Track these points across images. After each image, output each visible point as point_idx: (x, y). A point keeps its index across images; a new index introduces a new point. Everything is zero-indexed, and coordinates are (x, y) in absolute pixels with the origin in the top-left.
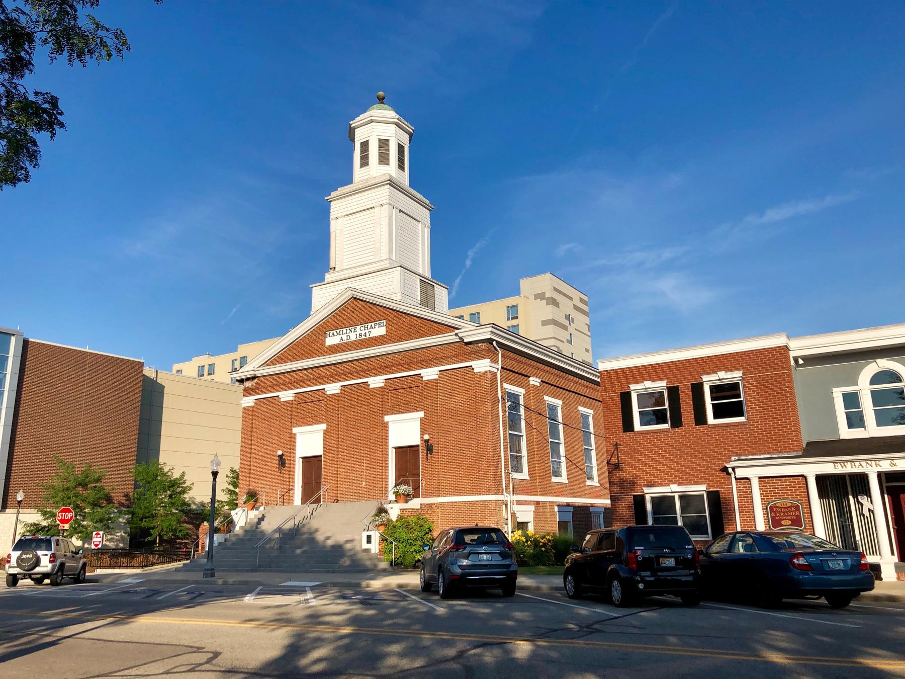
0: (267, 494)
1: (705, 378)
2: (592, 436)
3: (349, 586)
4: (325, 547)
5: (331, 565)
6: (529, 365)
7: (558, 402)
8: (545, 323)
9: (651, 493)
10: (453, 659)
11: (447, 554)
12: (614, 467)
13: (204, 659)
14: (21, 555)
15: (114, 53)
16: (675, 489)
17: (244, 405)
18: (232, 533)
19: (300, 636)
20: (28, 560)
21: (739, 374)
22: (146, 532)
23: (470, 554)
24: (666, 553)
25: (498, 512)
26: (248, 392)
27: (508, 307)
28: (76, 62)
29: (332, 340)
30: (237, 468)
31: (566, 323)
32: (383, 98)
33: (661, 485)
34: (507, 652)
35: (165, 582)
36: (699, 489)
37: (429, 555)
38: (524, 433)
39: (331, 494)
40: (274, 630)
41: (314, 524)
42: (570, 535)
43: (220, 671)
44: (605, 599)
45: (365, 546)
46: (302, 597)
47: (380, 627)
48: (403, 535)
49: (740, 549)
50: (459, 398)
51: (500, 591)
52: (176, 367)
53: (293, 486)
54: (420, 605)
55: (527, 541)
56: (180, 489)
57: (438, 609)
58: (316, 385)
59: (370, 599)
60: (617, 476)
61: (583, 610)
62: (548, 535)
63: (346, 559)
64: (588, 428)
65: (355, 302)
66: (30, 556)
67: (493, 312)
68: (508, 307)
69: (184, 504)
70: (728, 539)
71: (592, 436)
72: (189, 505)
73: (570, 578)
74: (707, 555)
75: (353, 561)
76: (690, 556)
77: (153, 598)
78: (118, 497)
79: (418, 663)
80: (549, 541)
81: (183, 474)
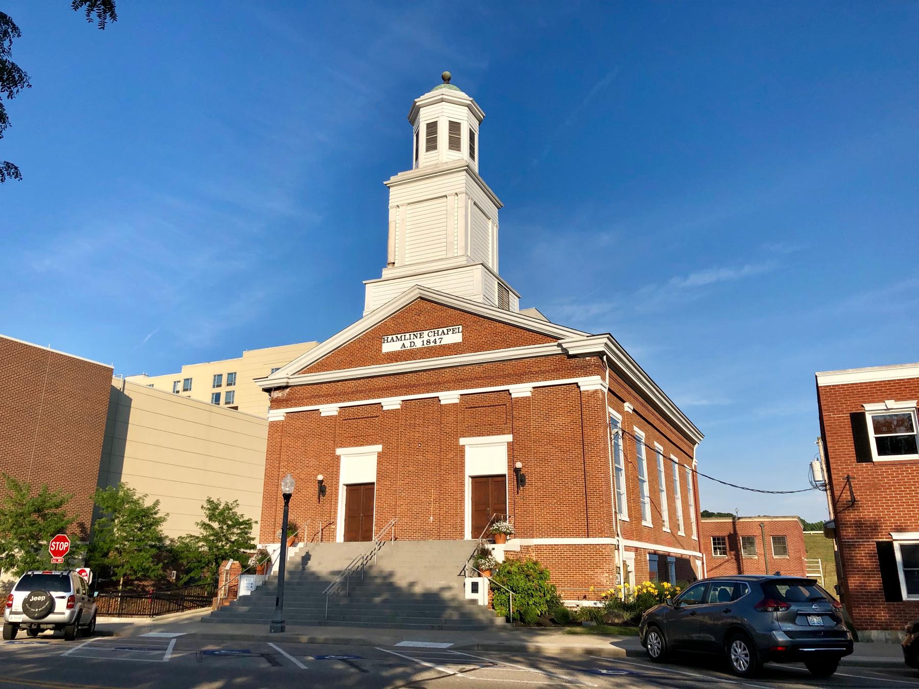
4: (413, 595)
9: (900, 539)
14: (30, 596)
17: (271, 419)
20: (39, 604)
21: (913, 404)
25: (610, 558)
26: (276, 404)
29: (389, 347)
32: (449, 79)
41: (386, 565)
45: (469, 595)
48: (522, 583)
50: (559, 421)
66: (43, 598)
75: (463, 615)
81: (157, 503)
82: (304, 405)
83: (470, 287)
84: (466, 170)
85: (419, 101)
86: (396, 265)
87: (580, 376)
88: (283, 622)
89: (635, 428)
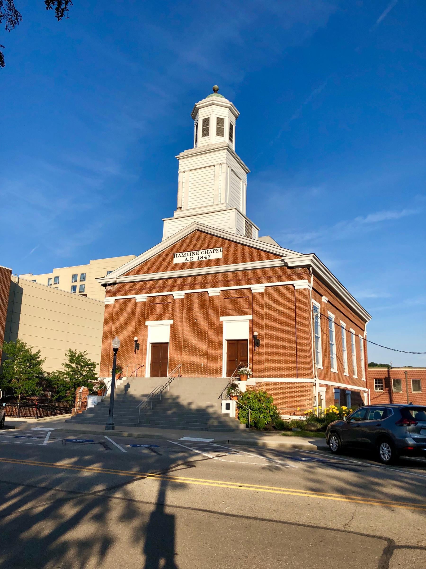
4: (191, 410)
17: (106, 303)
26: (109, 294)
27: (73, 275)
29: (178, 260)
32: (217, 90)
45: (224, 411)
48: (256, 405)
50: (281, 307)
68: (73, 275)
81: (39, 351)
84: (227, 149)
86: (182, 209)
88: (113, 424)
89: (329, 312)
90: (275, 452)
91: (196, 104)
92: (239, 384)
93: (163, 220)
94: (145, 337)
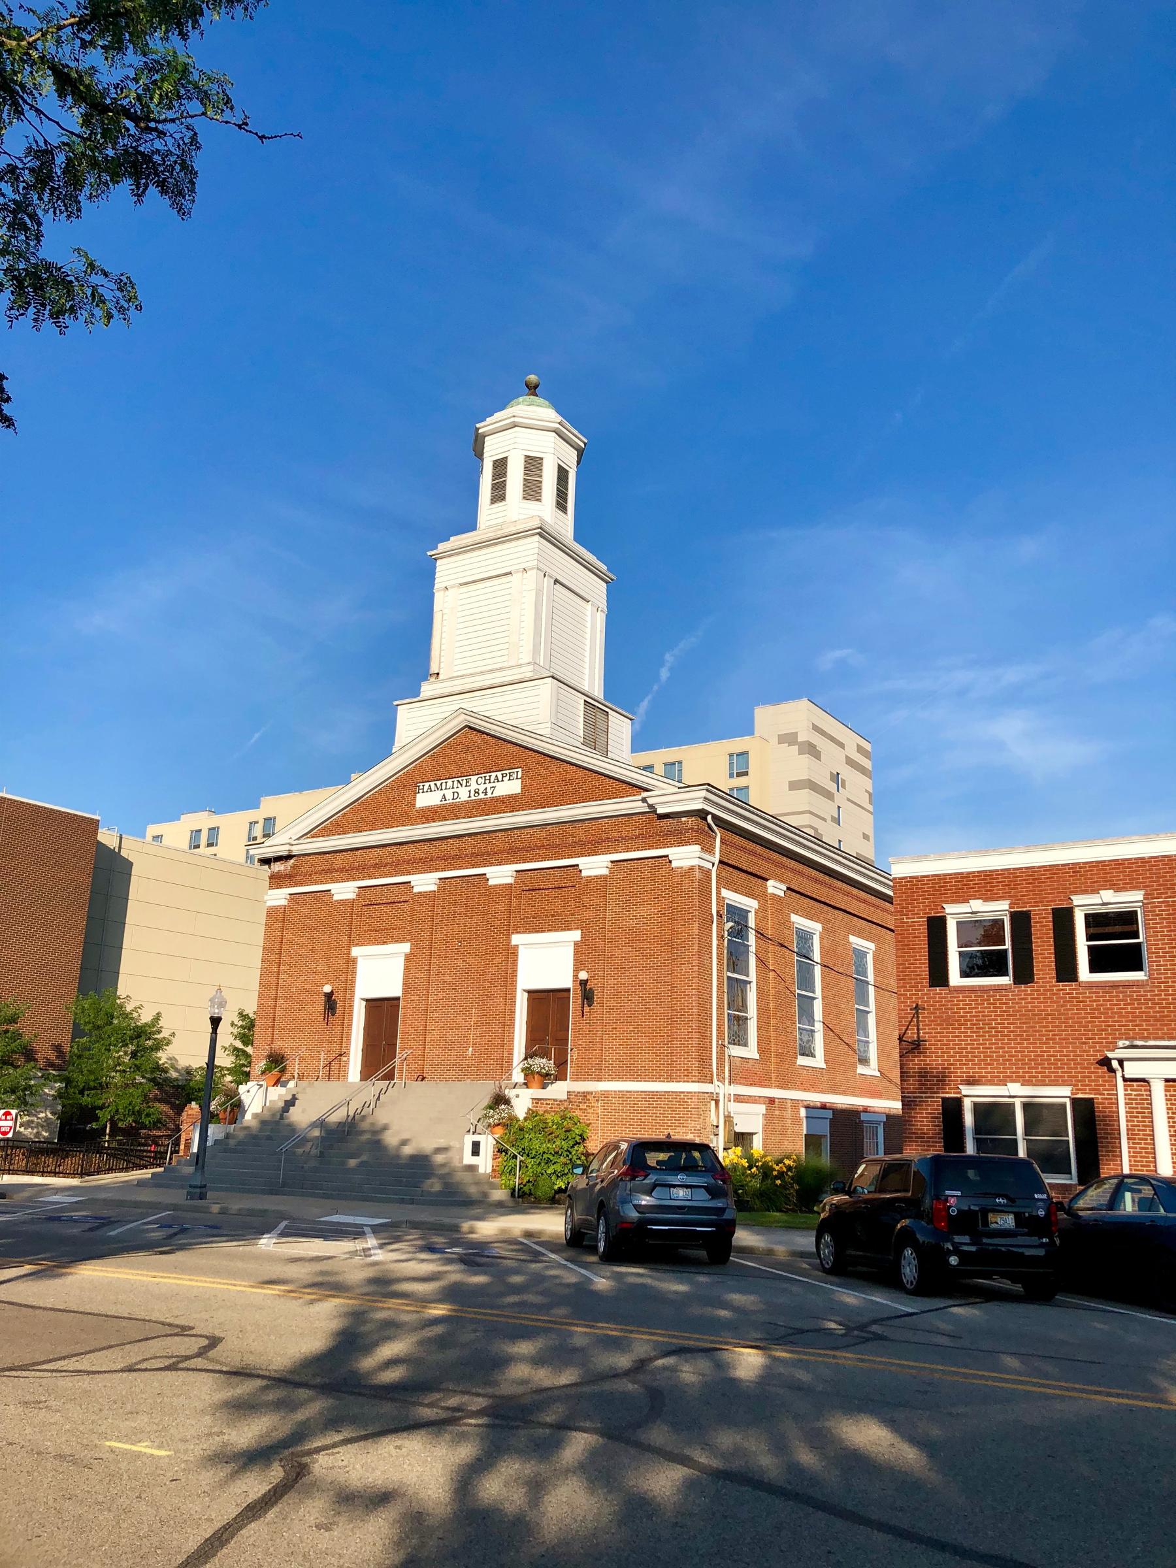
0: (302, 1060)
1: (1077, 900)
2: (871, 989)
3: (440, 1228)
4: (398, 1157)
5: (412, 1192)
6: (767, 859)
7: (815, 927)
8: (794, 786)
9: (973, 1095)
10: (627, 1373)
11: (614, 1183)
12: (911, 1047)
13: (195, 1349)
15: (114, 312)
16: (1015, 1092)
17: (269, 904)
18: (238, 1125)
19: (357, 1316)
22: (89, 1113)
23: (655, 1186)
24: (1000, 1205)
25: (702, 1113)
26: (277, 881)
27: (731, 755)
28: (48, 325)
29: (426, 799)
30: (251, 1009)
31: (832, 787)
32: (536, 387)
33: (991, 1083)
34: (720, 1366)
35: (121, 1203)
36: (1059, 1094)
37: (582, 1183)
38: (753, 976)
39: (413, 1066)
40: (312, 1302)
41: (382, 1116)
42: (825, 1160)
43: (221, 1372)
44: (889, 1279)
45: (469, 1159)
46: (358, 1245)
47: (499, 1307)
48: (536, 1145)
49: (1129, 1204)
50: (644, 911)
51: (703, 1254)
52: (152, 830)
53: (348, 1047)
54: (565, 1272)
55: (750, 1167)
56: (150, 1043)
57: (596, 1279)
58: (396, 874)
59: (476, 1256)
60: (915, 1063)
61: (850, 1297)
62: (789, 1158)
63: (434, 1180)
64: (865, 974)
65: (472, 736)
67: (706, 762)
68: (731, 755)
69: (158, 1068)
70: (1109, 1186)
71: (871, 989)
72: (166, 1071)
73: (827, 1238)
74: (1070, 1212)
75: (447, 1185)
76: (1041, 1213)
77: (99, 1233)
78: (44, 1052)
79: (567, 1377)
80: (789, 1168)
81: (158, 1017)
82: (312, 884)
83: (534, 712)
84: (539, 534)
85: (483, 427)
86: (441, 677)
87: (672, 845)
88: (205, 1186)
90: (515, 1247)
91: (478, 426)
92: (517, 1096)
93: (395, 703)
94: (349, 984)
